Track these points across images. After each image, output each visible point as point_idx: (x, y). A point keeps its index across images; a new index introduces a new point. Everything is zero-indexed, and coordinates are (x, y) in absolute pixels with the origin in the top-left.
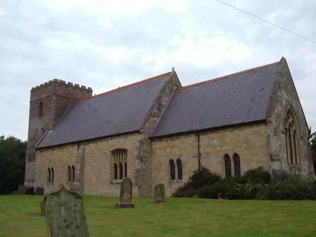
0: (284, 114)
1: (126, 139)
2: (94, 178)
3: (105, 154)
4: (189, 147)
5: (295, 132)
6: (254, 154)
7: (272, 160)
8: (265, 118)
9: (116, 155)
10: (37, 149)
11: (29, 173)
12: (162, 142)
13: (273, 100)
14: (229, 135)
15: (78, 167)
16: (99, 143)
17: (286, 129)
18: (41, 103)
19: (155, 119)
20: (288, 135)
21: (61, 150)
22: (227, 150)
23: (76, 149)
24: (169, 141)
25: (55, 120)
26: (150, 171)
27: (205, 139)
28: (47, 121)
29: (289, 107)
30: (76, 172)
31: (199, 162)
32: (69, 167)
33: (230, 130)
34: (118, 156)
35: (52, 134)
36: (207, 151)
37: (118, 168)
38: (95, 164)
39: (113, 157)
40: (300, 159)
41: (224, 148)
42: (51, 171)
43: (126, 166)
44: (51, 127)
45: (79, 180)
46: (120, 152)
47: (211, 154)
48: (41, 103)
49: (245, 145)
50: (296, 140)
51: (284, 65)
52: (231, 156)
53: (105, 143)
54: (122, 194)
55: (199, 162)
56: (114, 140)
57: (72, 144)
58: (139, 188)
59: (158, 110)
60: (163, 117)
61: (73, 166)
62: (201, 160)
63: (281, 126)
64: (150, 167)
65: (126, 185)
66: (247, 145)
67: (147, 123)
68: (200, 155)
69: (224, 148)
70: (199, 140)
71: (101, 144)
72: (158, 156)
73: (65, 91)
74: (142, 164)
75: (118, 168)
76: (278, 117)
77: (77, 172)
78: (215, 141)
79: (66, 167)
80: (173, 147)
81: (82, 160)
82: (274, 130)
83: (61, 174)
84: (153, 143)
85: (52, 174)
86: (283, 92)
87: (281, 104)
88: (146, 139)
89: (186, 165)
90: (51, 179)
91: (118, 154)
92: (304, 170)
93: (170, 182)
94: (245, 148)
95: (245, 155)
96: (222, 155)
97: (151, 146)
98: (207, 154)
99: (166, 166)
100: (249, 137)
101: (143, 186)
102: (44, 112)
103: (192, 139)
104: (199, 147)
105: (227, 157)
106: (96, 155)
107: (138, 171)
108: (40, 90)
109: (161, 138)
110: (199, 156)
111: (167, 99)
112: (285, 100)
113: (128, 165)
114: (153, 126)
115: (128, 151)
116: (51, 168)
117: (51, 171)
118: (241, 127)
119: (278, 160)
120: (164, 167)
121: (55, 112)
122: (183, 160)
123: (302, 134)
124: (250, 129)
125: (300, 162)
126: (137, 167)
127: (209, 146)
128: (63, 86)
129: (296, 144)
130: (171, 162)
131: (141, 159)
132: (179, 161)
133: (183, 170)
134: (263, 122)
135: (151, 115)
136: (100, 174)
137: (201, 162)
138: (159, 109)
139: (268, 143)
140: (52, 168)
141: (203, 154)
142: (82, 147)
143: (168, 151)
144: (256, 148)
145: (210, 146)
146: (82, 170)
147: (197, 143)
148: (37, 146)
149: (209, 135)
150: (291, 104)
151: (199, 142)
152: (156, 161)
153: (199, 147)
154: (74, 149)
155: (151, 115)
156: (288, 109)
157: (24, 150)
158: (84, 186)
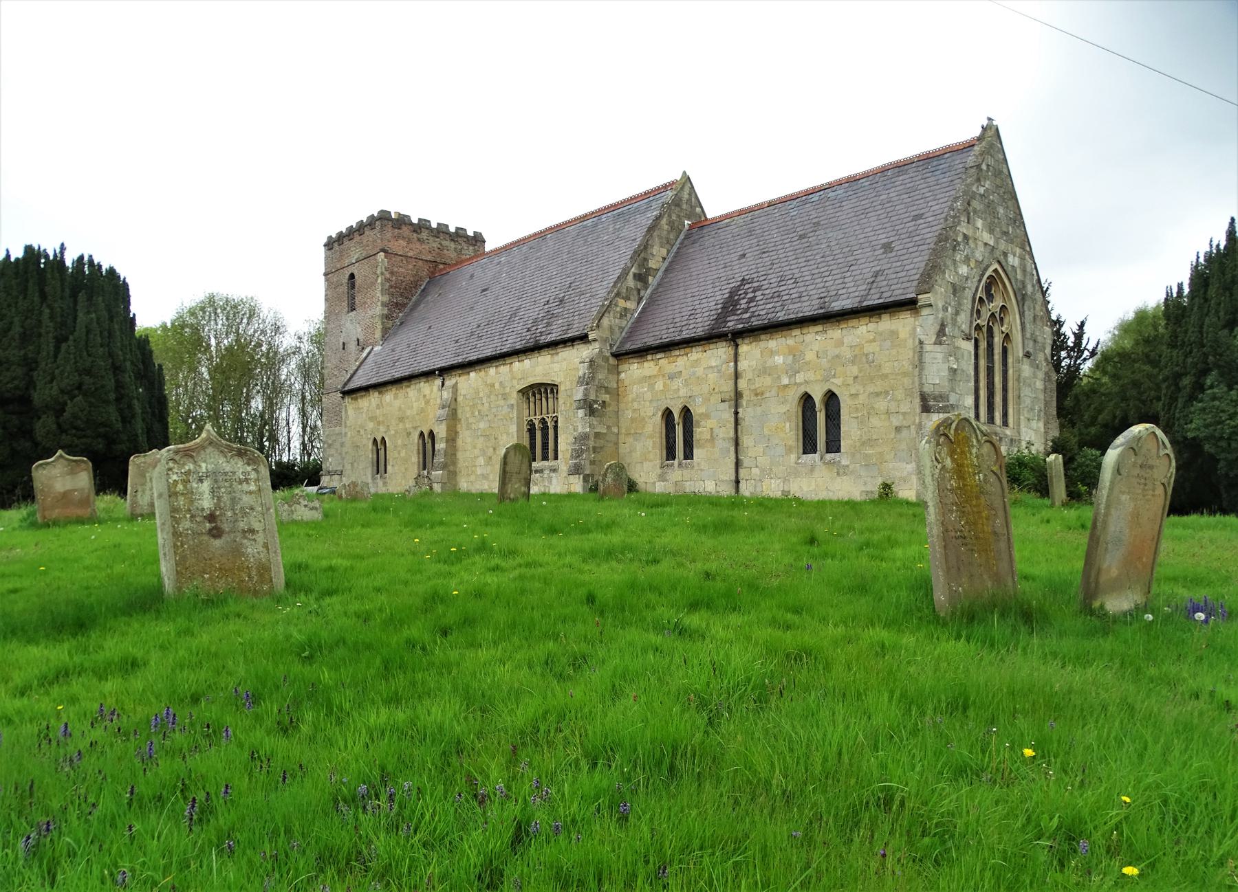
0: (974, 287)
1: (556, 358)
2: (481, 461)
3: (505, 397)
4: (712, 376)
5: (1007, 337)
6: (878, 394)
7: (926, 409)
8: (913, 295)
9: (532, 399)
10: (346, 393)
11: (332, 456)
13: (1211, 246)
14: (815, 340)
15: (441, 431)
16: (492, 371)
17: (978, 328)
19: (630, 305)
20: (983, 345)
21: (401, 393)
22: (806, 382)
23: (435, 388)
24: (663, 362)
26: (613, 438)
29: (996, 266)
31: (736, 413)
32: (422, 434)
33: (819, 328)
35: (379, 353)
36: (757, 386)
38: (482, 425)
39: (525, 406)
41: (799, 378)
42: (380, 446)
43: (556, 427)
44: (378, 334)
45: (444, 466)
46: (541, 391)
47: (767, 395)
48: (352, 276)
49: (854, 370)
50: (1010, 360)
51: (991, 146)
52: (818, 398)
53: (504, 369)
55: (736, 413)
56: (527, 362)
57: (428, 374)
60: (652, 301)
62: (740, 410)
63: (963, 319)
64: (615, 430)
68: (738, 395)
70: (736, 355)
72: (633, 400)
74: (594, 421)
77: (440, 446)
78: (779, 360)
79: (416, 435)
80: (672, 377)
81: (452, 414)
83: (403, 454)
84: (623, 367)
85: (382, 453)
89: (703, 423)
90: (380, 466)
91: (538, 396)
93: (662, 467)
94: (856, 378)
95: (854, 396)
96: (794, 396)
97: (619, 373)
99: (655, 425)
100: (869, 348)
103: (719, 353)
104: (737, 376)
105: (807, 399)
106: (484, 401)
107: (583, 438)
108: (346, 242)
109: (642, 353)
110: (737, 401)
113: (559, 425)
115: (562, 388)
117: (380, 446)
122: (696, 411)
124: (872, 326)
126: (580, 430)
128: (404, 228)
129: (1010, 372)
130: (668, 414)
131: (590, 407)
132: (686, 412)
133: (696, 436)
134: (910, 305)
135: (618, 295)
136: (494, 449)
137: (740, 415)
138: (641, 278)
139: (920, 363)
140: (383, 438)
141: (746, 394)
142: (449, 382)
143: (659, 385)
145: (765, 372)
146: (452, 439)
147: (732, 364)
149: (762, 344)
151: (736, 361)
152: (629, 414)
153: (737, 376)
154: (431, 388)
155: (618, 295)
156: (989, 272)
158: (458, 478)
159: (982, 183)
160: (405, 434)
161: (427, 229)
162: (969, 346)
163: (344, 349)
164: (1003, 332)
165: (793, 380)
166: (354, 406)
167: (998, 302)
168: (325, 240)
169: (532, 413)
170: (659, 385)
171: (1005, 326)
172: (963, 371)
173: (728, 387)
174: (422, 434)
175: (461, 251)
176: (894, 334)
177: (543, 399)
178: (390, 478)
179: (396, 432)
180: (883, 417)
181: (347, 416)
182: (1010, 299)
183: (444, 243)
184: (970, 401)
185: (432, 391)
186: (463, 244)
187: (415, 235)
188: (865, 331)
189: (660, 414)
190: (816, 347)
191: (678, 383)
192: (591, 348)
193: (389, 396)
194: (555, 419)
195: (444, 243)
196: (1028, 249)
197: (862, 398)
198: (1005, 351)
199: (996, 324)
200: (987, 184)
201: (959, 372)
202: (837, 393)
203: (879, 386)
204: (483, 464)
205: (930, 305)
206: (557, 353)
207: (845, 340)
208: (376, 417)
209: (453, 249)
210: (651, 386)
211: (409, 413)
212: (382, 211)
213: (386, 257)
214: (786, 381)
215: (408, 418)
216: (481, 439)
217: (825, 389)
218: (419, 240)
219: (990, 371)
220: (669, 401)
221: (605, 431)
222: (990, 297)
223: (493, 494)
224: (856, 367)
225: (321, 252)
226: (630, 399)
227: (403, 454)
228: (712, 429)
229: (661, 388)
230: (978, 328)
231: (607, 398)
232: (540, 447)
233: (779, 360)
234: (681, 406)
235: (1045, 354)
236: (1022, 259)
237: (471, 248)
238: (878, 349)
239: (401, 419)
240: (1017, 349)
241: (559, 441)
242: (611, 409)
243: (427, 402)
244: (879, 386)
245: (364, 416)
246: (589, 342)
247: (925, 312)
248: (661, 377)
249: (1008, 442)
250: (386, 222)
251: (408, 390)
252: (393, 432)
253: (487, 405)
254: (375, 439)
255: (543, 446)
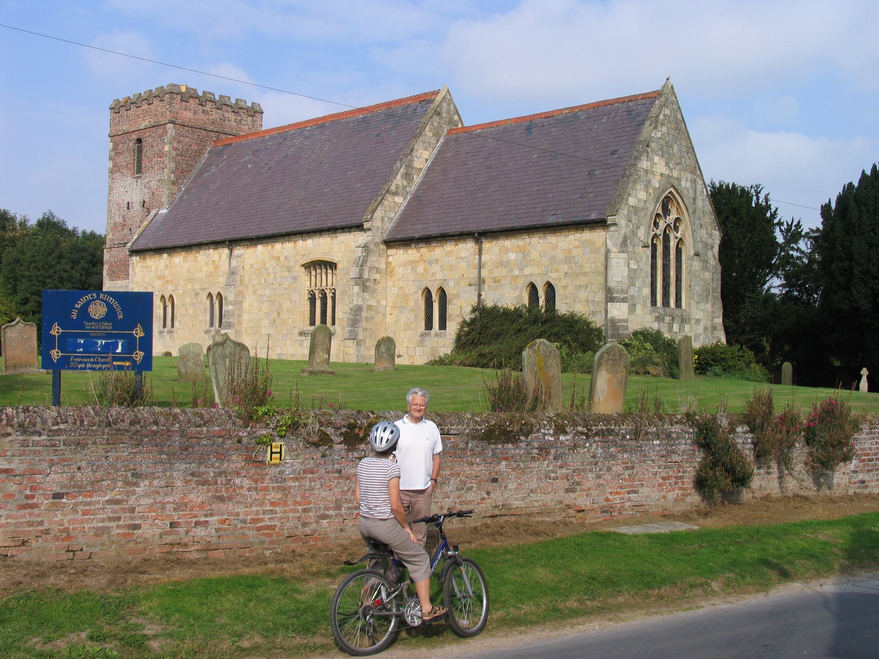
1: (335, 240)
2: (266, 323)
3: (289, 269)
6: (580, 287)
9: (313, 273)
10: (134, 252)
12: (410, 251)
14: (537, 243)
16: (278, 246)
18: (139, 141)
22: (532, 274)
25: (173, 183)
27: (491, 247)
28: (154, 184)
30: (224, 308)
34: (318, 276)
37: (318, 303)
38: (268, 292)
39: (308, 278)
40: (689, 297)
43: (334, 299)
48: (139, 141)
49: (565, 268)
50: (684, 258)
54: (312, 352)
55: (480, 295)
58: (357, 345)
59: (406, 179)
61: (219, 293)
62: (483, 293)
63: (641, 233)
64: (383, 303)
65: (320, 337)
66: (570, 268)
67: (379, 208)
69: (527, 271)
71: (281, 248)
73: (195, 113)
75: (318, 303)
76: (636, 214)
82: (621, 240)
83: (191, 311)
85: (169, 309)
86: (656, 159)
87: (648, 184)
88: (376, 244)
89: (454, 301)
92: (698, 321)
94: (566, 273)
95: (565, 287)
98: (495, 282)
101: (367, 342)
102: (145, 163)
103: (468, 247)
104: (480, 267)
111: (426, 154)
112: (658, 177)
113: (337, 297)
114: (392, 215)
115: (339, 266)
116: (167, 297)
118: (561, 229)
119: (624, 300)
120: (411, 304)
121: (173, 165)
123: (700, 245)
125: (689, 305)
126: (355, 302)
127: (501, 264)
128: (192, 101)
130: (428, 293)
131: (362, 282)
140: (171, 296)
143: (420, 269)
144: (585, 274)
145: (502, 265)
147: (477, 256)
148: (133, 244)
150: (675, 183)
151: (480, 254)
153: (480, 267)
157: (811, 530)
159: (659, 129)
160: (193, 294)
161: (211, 101)
162: (649, 251)
163: (128, 208)
164: (676, 238)
165: (521, 272)
166: (142, 264)
167: (673, 216)
168: (111, 103)
169: (313, 284)
170: (420, 269)
171: (680, 233)
172: (641, 270)
173: (474, 274)
174: (210, 295)
175: (240, 121)
176: (591, 242)
177: (323, 273)
178: (176, 332)
179: (185, 292)
180: (584, 303)
181: (135, 274)
182: (683, 214)
183: (227, 115)
184: (647, 291)
185: (220, 257)
186: (243, 115)
187: (200, 107)
188: (573, 239)
189: (420, 292)
190: (539, 248)
191: (436, 268)
192: (365, 235)
193: (178, 259)
194: (333, 291)
195: (227, 115)
196: (699, 173)
197: (570, 289)
198: (679, 251)
199: (672, 232)
200: (664, 129)
201: (639, 271)
202: (553, 284)
203: (582, 280)
204: (267, 325)
205: (615, 224)
206: (337, 237)
207: (559, 245)
208: (165, 277)
209: (233, 120)
210: (414, 269)
211: (197, 275)
212: (174, 85)
213: (174, 128)
214: (517, 273)
215: (196, 280)
216: (267, 304)
217: (545, 281)
218: (203, 112)
219: (666, 267)
220: (428, 282)
221: (375, 304)
222: (666, 211)
223: (305, 361)
224: (566, 266)
225: (108, 115)
226: (396, 279)
227: (191, 311)
228: (461, 307)
229: (422, 271)
230: (655, 236)
231: (377, 276)
232: (320, 316)
233: (512, 256)
234: (437, 287)
235: (713, 252)
236: (694, 182)
237: (250, 119)
238: (582, 253)
239: (190, 280)
240: (688, 251)
241: (336, 311)
242: (380, 286)
243: (216, 267)
244: (582, 280)
245: (152, 274)
246: (365, 231)
247: (612, 228)
248: (422, 263)
249: (679, 320)
250: (175, 96)
251: (197, 255)
252: (181, 292)
253: (272, 275)
254: (163, 296)
255: (322, 313)
